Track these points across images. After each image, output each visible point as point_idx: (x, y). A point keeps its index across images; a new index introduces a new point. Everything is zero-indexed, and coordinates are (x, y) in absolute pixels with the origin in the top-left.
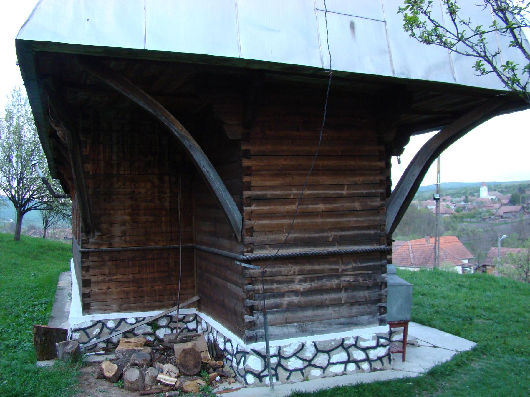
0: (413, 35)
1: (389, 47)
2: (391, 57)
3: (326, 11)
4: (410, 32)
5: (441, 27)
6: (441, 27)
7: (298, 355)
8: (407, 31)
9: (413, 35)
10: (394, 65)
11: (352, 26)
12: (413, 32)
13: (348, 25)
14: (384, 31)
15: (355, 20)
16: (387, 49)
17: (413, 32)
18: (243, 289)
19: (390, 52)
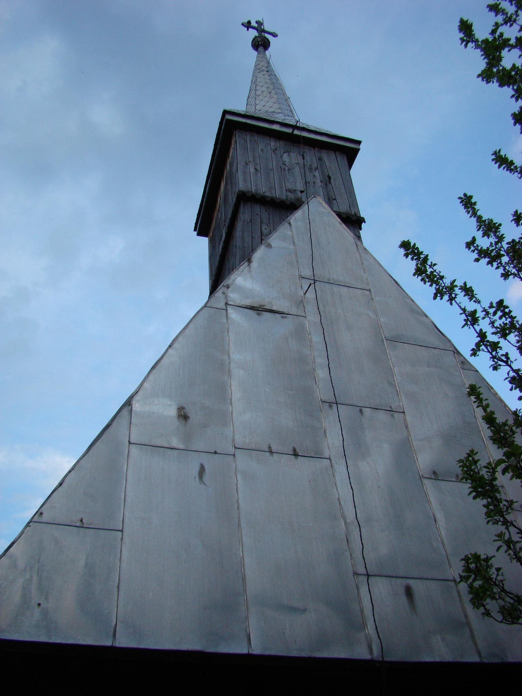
0: (487, 613)
1: (466, 616)
2: (471, 631)
3: (368, 575)
4: (482, 609)
5: (515, 527)
6: (515, 527)
7: (207, 305)
8: (477, 608)
9: (487, 613)
10: (478, 642)
11: (409, 592)
12: (485, 609)
13: (402, 591)
14: (455, 593)
15: (412, 583)
16: (463, 619)
17: (485, 609)
18: (502, 25)
19: (468, 624)
